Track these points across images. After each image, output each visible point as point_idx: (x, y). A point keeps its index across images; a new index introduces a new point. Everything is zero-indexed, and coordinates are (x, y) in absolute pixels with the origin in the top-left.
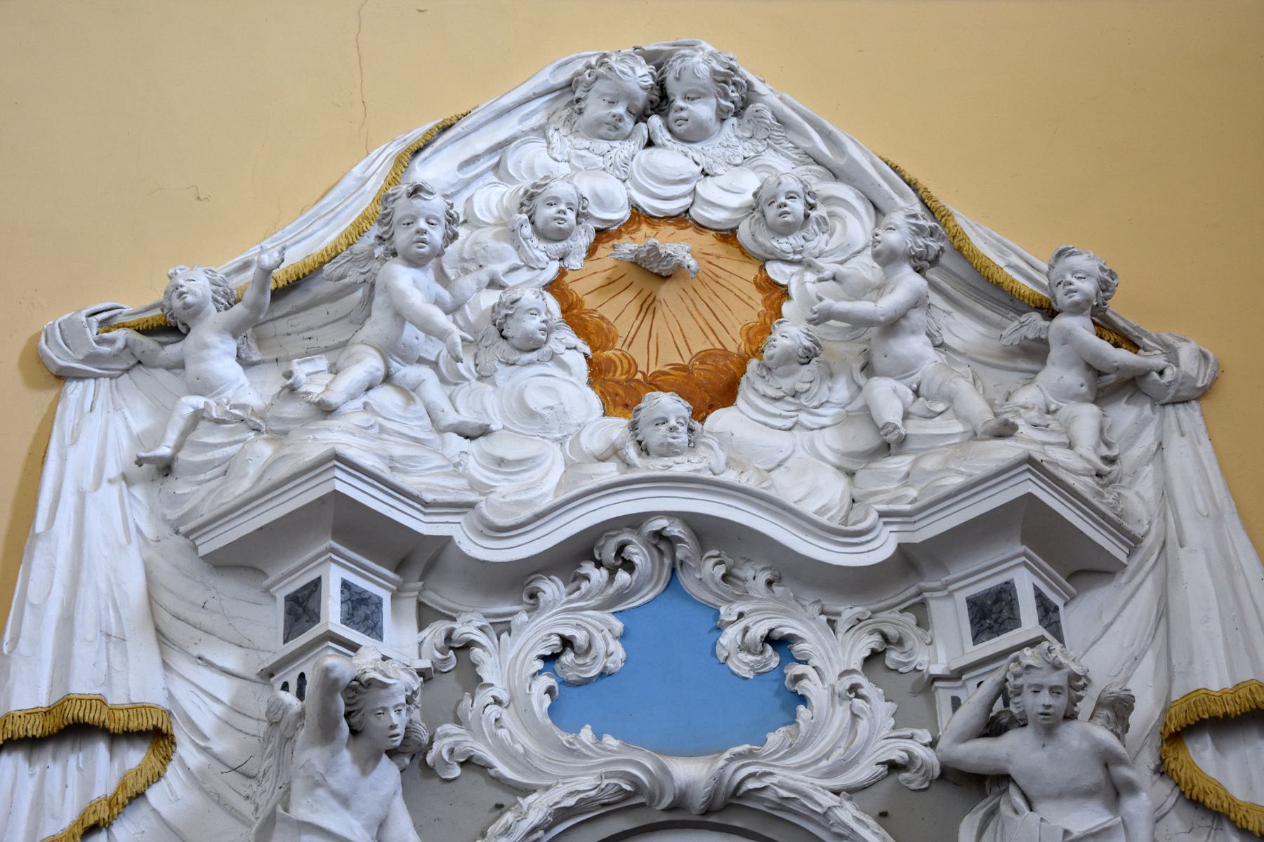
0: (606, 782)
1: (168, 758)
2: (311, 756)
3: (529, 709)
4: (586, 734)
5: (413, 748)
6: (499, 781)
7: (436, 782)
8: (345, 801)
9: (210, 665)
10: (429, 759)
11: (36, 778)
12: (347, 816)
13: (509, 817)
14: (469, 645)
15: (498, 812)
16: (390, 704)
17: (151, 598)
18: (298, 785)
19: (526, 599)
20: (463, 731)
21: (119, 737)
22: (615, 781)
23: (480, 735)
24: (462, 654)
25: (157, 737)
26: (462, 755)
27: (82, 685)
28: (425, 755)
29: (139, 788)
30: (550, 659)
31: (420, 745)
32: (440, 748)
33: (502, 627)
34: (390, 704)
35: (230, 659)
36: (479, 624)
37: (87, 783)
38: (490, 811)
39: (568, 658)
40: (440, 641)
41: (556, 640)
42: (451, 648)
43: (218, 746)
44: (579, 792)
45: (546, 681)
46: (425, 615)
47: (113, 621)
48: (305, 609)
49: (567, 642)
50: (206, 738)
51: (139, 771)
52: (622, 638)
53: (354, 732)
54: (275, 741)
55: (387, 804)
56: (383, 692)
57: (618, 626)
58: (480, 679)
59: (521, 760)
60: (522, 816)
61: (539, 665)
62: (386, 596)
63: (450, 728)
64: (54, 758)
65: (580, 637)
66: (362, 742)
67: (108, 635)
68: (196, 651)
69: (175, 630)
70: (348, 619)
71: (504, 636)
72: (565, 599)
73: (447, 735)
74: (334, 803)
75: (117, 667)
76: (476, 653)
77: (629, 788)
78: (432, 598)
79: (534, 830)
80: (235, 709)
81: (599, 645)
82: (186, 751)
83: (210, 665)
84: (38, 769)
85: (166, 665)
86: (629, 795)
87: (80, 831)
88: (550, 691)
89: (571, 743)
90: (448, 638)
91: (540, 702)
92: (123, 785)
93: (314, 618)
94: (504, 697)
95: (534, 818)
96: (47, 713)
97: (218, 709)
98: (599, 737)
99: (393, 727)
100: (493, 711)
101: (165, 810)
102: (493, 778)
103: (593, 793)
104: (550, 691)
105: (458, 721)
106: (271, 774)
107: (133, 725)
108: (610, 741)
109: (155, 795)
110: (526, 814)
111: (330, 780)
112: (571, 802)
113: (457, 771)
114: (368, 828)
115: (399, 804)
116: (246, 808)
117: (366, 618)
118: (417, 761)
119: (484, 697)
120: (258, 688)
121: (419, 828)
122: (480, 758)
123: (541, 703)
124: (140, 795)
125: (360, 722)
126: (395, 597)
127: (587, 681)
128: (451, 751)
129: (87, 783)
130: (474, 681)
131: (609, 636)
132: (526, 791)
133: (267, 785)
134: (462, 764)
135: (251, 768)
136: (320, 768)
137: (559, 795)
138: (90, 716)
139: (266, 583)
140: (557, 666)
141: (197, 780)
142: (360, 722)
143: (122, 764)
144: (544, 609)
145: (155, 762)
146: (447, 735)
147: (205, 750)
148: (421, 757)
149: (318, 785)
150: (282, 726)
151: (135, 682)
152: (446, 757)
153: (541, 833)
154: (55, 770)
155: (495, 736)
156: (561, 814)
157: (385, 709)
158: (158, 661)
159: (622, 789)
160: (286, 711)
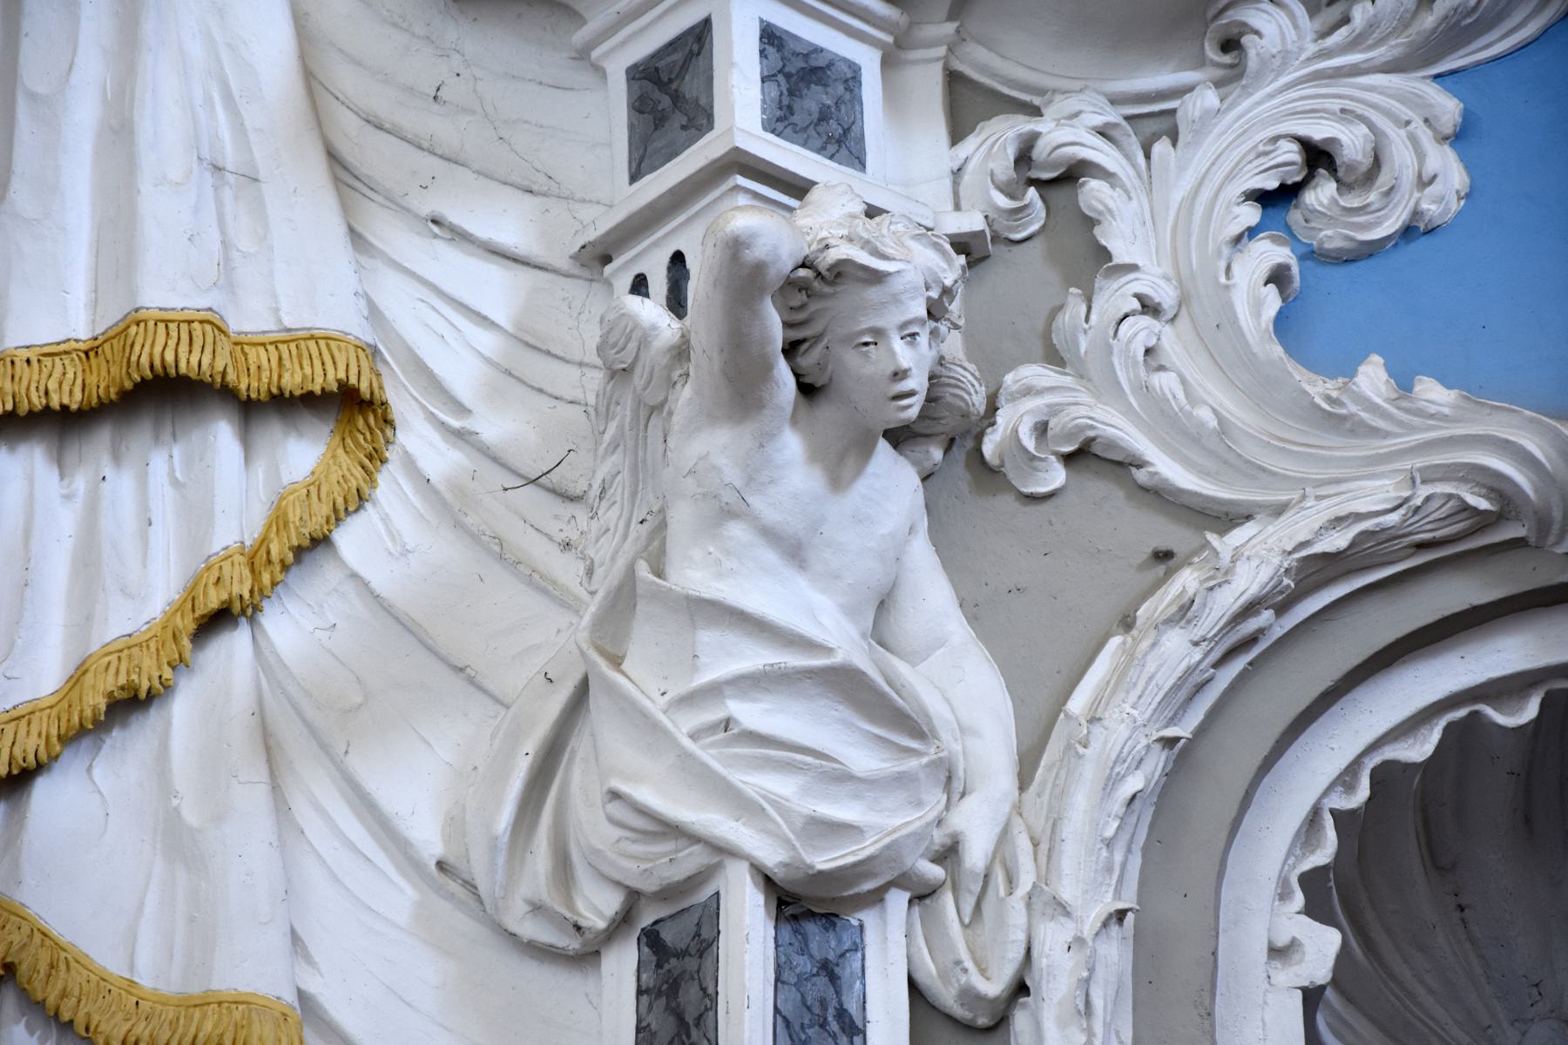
0: (1424, 491)
1: (376, 457)
2: (707, 447)
3: (1227, 322)
4: (1373, 378)
5: (949, 423)
6: (1160, 497)
7: (1007, 502)
8: (794, 551)
9: (459, 236)
10: (988, 448)
11: (79, 503)
12: (801, 582)
13: (1187, 580)
14: (1073, 174)
15: (1161, 569)
16: (889, 320)
17: (310, 78)
18: (682, 516)
19: (1212, 53)
20: (1068, 381)
21: (262, 409)
22: (1448, 488)
23: (1110, 389)
24: (1059, 195)
25: (351, 407)
26: (1068, 436)
27: (164, 290)
28: (979, 438)
29: (315, 525)
30: (1276, 199)
31: (965, 415)
32: (1014, 422)
33: (1155, 124)
34: (889, 320)
35: (507, 222)
36: (1098, 120)
37: (197, 514)
38: (1142, 567)
39: (1322, 193)
40: (1004, 165)
41: (1290, 153)
42: (1033, 182)
43: (493, 427)
44: (1359, 517)
45: (1269, 253)
46: (966, 104)
47: (226, 134)
48: (677, 98)
49: (1318, 157)
50: (461, 409)
51: (313, 486)
52: (1458, 138)
53: (808, 390)
54: (625, 412)
55: (897, 558)
56: (873, 293)
57: (1449, 108)
58: (1104, 254)
59: (1215, 446)
60: (1220, 577)
61: (1251, 214)
62: (868, 60)
63: (1035, 373)
64: (117, 458)
65: (1352, 143)
66: (827, 412)
67: (218, 169)
68: (427, 205)
69: (374, 155)
70: (781, 120)
71: (1161, 148)
72: (1312, 48)
73: (1028, 391)
74: (770, 556)
75: (244, 243)
76: (1093, 191)
77: (1483, 504)
78: (979, 62)
79: (1250, 609)
80: (527, 341)
81: (1401, 158)
82: (416, 437)
83: (459, 236)
84: (80, 483)
85: (356, 237)
86: (1484, 522)
87: (188, 624)
88: (1278, 277)
89: (1329, 399)
90: (1024, 158)
91: (1256, 306)
92: (278, 520)
93: (700, 118)
94: (1166, 296)
95: (1249, 580)
96: (90, 352)
97: (487, 341)
98: (1404, 383)
99: (899, 375)
100: (1141, 330)
101: (380, 577)
102: (1145, 489)
103: (1394, 518)
104: (1278, 277)
105: (1054, 357)
106: (619, 491)
107: (292, 381)
108: (1433, 393)
109: (350, 539)
110: (1229, 571)
111: (757, 502)
112: (1338, 541)
113: (1056, 476)
114: (851, 611)
115: (921, 553)
116: (567, 571)
117: (824, 117)
118: (959, 454)
119: (1115, 296)
120: (576, 290)
121: (973, 611)
122: (1112, 444)
123: (1257, 306)
124: (320, 542)
125: (821, 366)
126: (889, 62)
127: (1370, 251)
128: (1042, 429)
129: (197, 514)
130: (1091, 261)
131: (1425, 136)
132: (1227, 518)
133: (611, 515)
134: (1068, 459)
135: (572, 477)
136: (732, 475)
137: (1310, 526)
138: (190, 362)
139: (581, 36)
140: (1295, 216)
141: (448, 506)
142: (821, 366)
143: (274, 471)
144: (1259, 76)
145: (349, 467)
146: (1028, 391)
147: (461, 437)
148: (970, 444)
149: (728, 514)
150: (638, 380)
151: (288, 284)
152: (1029, 443)
153: (1267, 616)
154: (121, 486)
155: (1145, 389)
156: (1316, 570)
157: (879, 333)
158: (340, 230)
159: (1466, 508)
160: (644, 342)
